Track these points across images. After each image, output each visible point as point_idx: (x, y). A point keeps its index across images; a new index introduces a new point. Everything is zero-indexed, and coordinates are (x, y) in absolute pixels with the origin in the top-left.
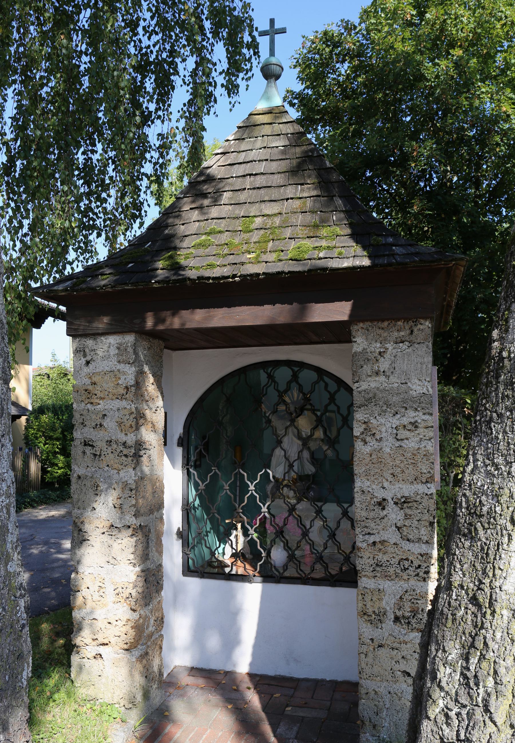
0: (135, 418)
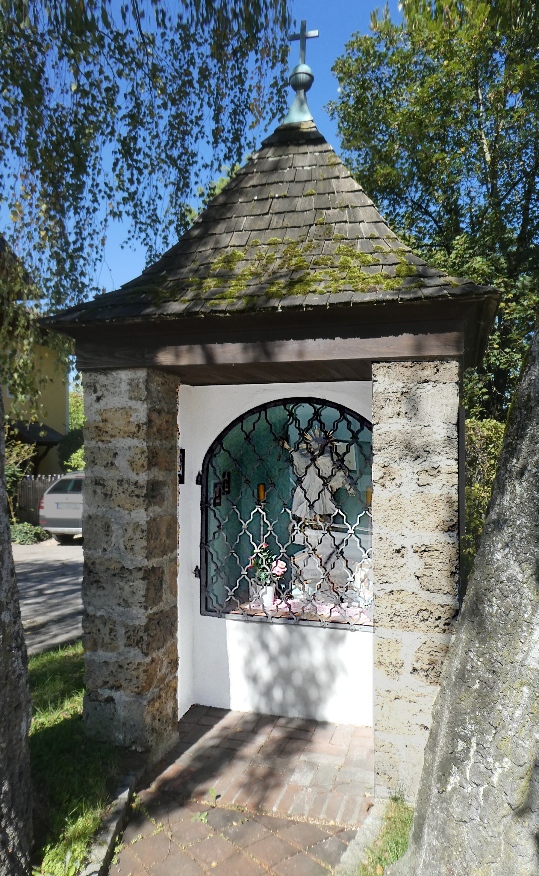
0: (147, 457)
